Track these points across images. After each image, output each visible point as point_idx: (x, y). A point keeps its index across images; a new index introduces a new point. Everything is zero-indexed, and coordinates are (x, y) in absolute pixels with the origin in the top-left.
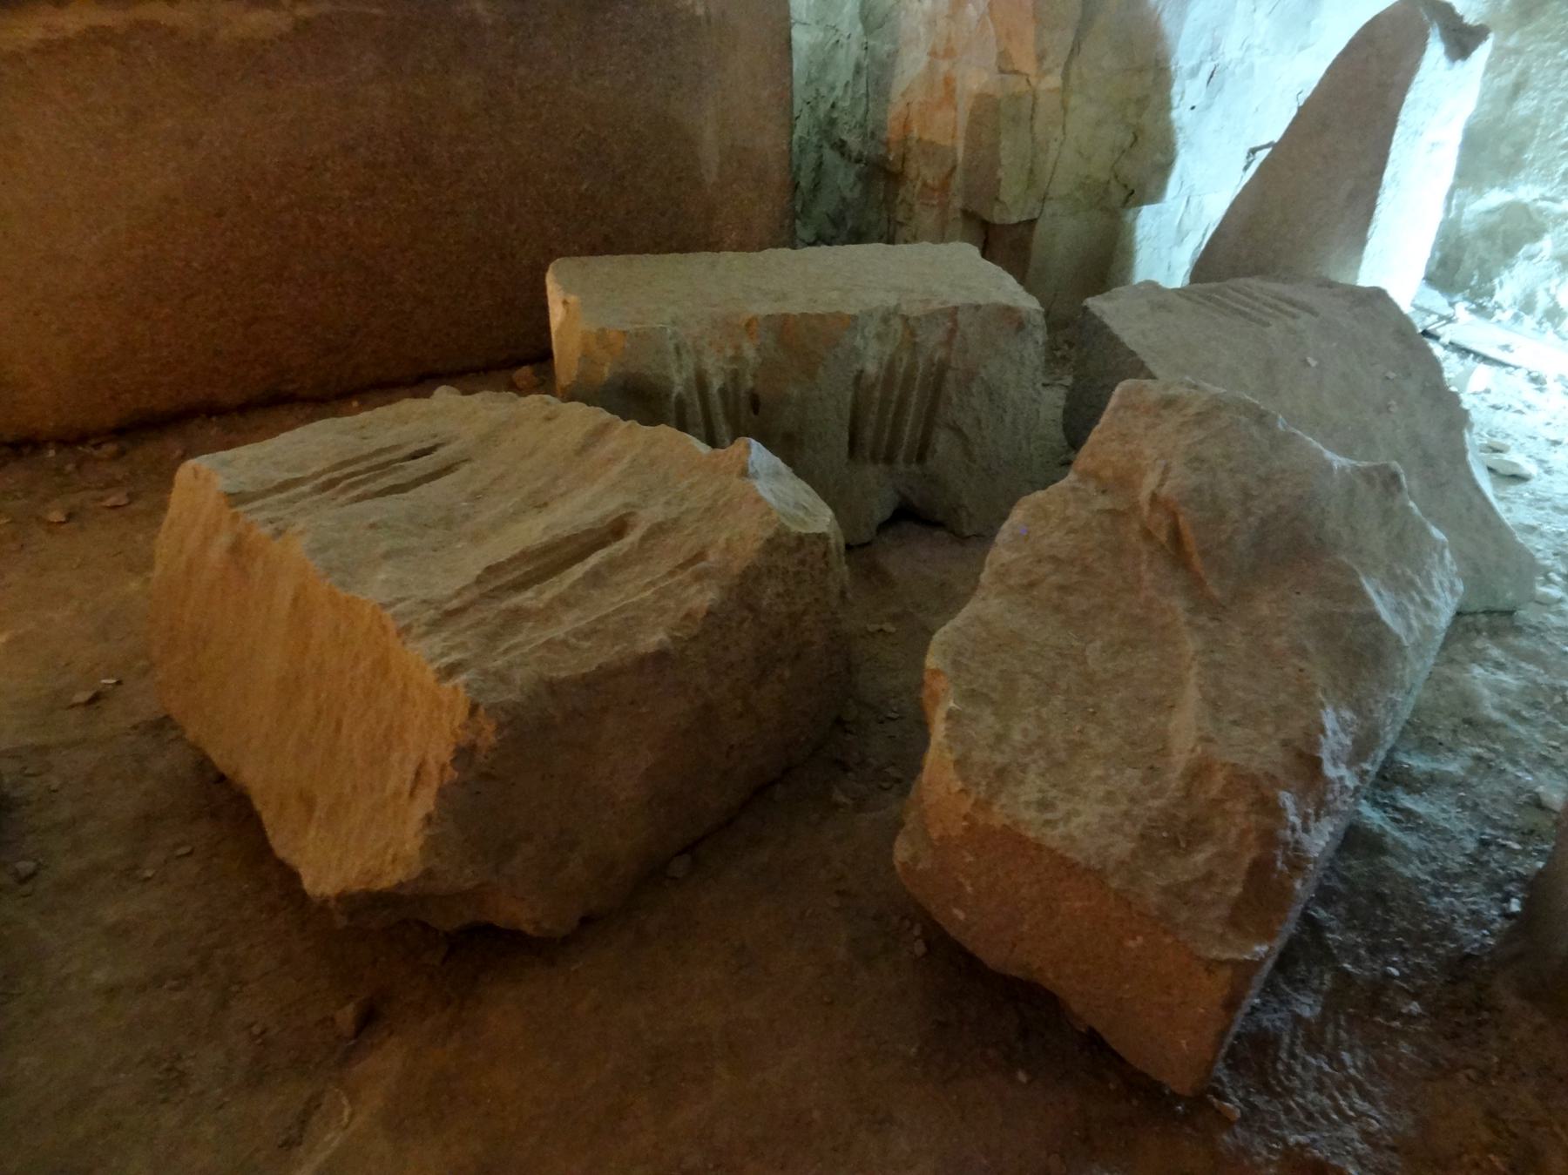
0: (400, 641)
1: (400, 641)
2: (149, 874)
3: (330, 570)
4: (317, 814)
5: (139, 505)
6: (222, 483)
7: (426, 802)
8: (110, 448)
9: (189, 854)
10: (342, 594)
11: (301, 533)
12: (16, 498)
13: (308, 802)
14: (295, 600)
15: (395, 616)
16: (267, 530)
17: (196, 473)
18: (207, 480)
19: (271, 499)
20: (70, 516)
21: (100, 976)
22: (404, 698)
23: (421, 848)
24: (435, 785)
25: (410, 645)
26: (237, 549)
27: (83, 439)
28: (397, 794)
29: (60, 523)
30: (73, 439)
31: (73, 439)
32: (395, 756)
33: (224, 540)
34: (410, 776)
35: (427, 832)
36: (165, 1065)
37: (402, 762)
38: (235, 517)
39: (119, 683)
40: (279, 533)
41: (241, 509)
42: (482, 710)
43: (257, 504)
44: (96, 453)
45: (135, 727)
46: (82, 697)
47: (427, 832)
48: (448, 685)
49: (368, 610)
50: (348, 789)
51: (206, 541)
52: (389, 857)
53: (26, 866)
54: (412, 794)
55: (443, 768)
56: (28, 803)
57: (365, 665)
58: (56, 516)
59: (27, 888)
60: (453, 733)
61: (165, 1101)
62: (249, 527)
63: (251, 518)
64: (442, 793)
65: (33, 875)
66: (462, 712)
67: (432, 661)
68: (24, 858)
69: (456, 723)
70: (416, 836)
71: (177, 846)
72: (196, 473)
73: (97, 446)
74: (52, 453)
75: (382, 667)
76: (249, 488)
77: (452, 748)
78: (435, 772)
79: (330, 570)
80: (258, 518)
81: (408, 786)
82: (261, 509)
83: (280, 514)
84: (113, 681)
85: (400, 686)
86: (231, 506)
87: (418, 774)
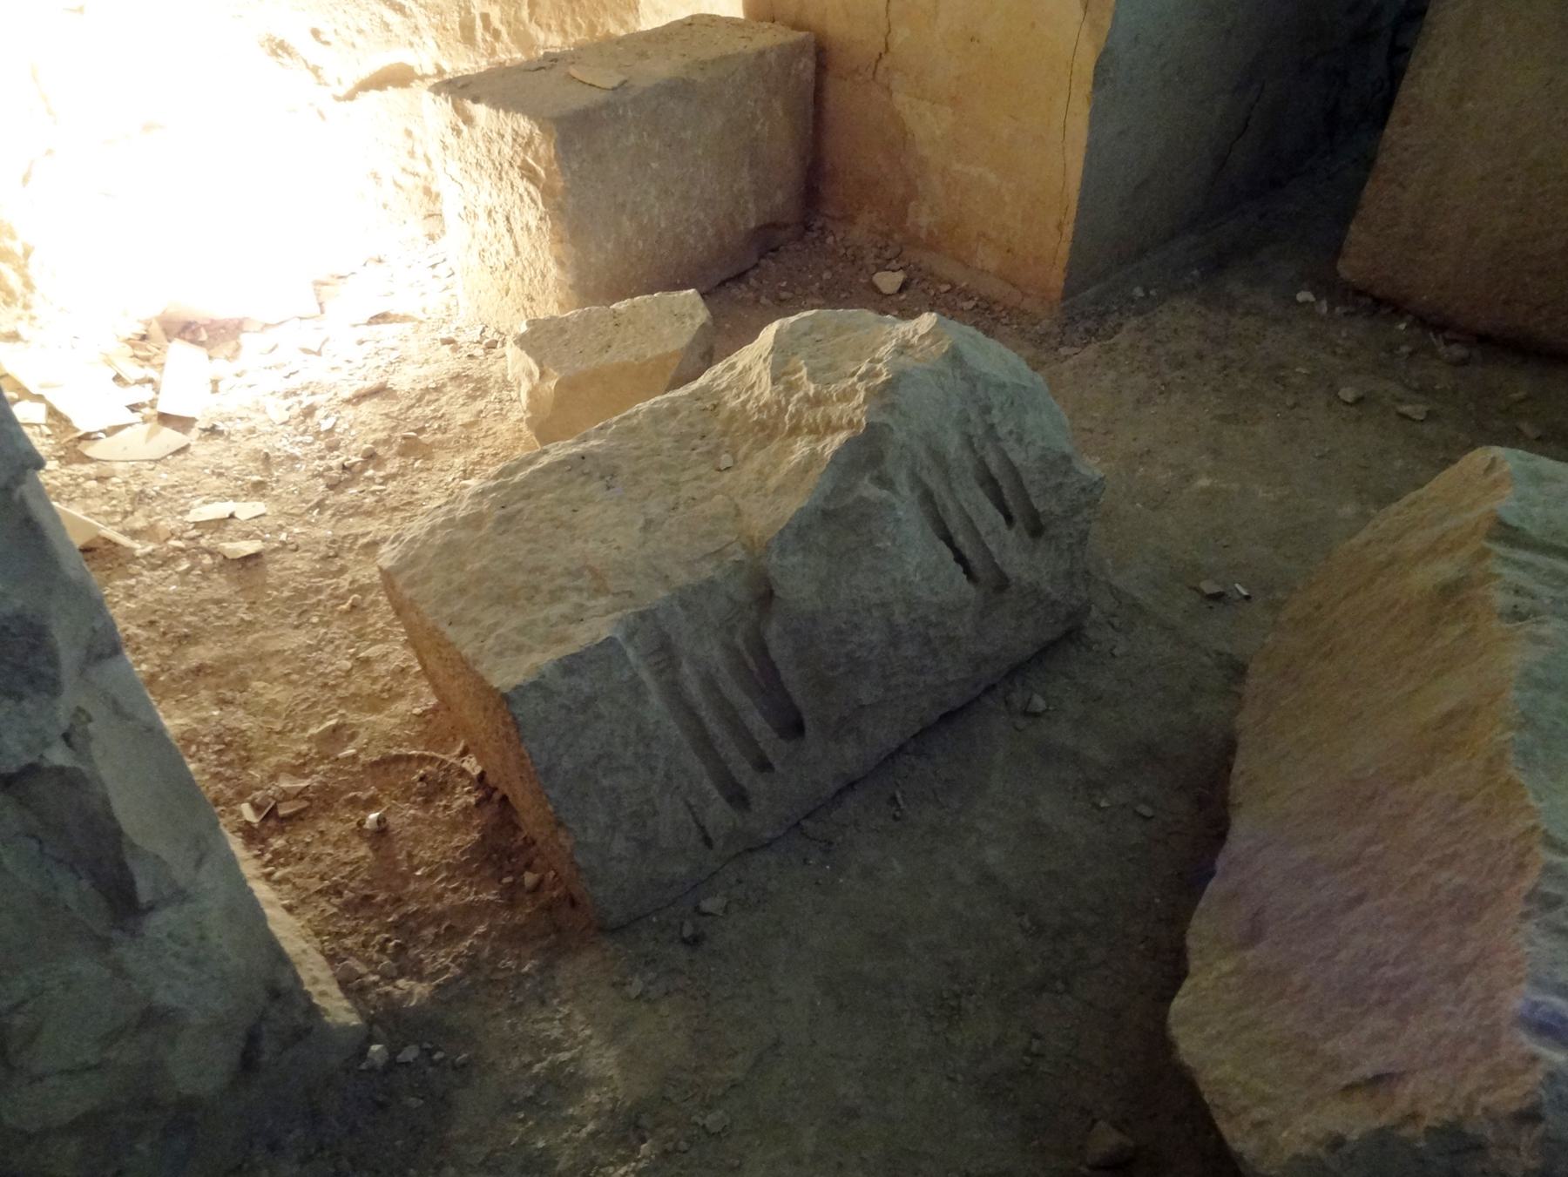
0: (1521, 908)
1: (1521, 908)
2: (1103, 804)
3: (1527, 722)
4: (1249, 954)
5: (1429, 430)
6: (1506, 504)
7: (1354, 1120)
8: (1458, 351)
9: (1146, 818)
10: (1512, 769)
11: (1539, 640)
12: (1334, 353)
13: (1253, 937)
14: (1450, 716)
15: (1549, 869)
16: (1501, 599)
17: (1492, 465)
18: (1496, 484)
19: (1542, 561)
20: (1359, 401)
21: (993, 856)
22: (1456, 975)
23: (1296, 1157)
24: (1384, 1120)
25: (1529, 926)
26: (1450, 593)
27: (1440, 328)
28: (1335, 1064)
29: (1347, 403)
30: (1434, 323)
31: (1434, 323)
32: (1377, 1022)
33: (1446, 569)
34: (1367, 1070)
35: (1321, 1151)
36: (956, 987)
37: (1379, 1038)
38: (1484, 554)
39: (1247, 598)
40: (1517, 615)
41: (1499, 549)
42: (1540, 1130)
43: (1523, 556)
44: (1442, 349)
45: (1219, 654)
46: (1209, 587)
47: (1321, 1151)
48: (1529, 1043)
49: (1521, 823)
50: (1297, 979)
51: (1432, 552)
52: (1257, 1114)
53: (1039, 703)
54: (1350, 1088)
55: (1414, 1117)
56: (1089, 649)
57: (1450, 878)
58: (1348, 394)
59: (1022, 723)
60: (1470, 1102)
61: (930, 1017)
62: (1489, 577)
63: (1498, 569)
64: (1382, 1138)
65: (1036, 715)
66: (1510, 1097)
67: (1538, 983)
68: (1044, 695)
69: (1484, 1100)
70: (1307, 1138)
71: (1145, 800)
72: (1492, 465)
73: (1448, 342)
74: (1402, 326)
75: (1469, 906)
76: (1533, 530)
77: (1447, 1115)
78: (1402, 1105)
79: (1527, 722)
80: (1508, 573)
81: (1355, 1075)
82: (1523, 566)
83: (1537, 588)
84: (1245, 593)
85: (1466, 954)
86: (1490, 537)
87: (1378, 1079)
